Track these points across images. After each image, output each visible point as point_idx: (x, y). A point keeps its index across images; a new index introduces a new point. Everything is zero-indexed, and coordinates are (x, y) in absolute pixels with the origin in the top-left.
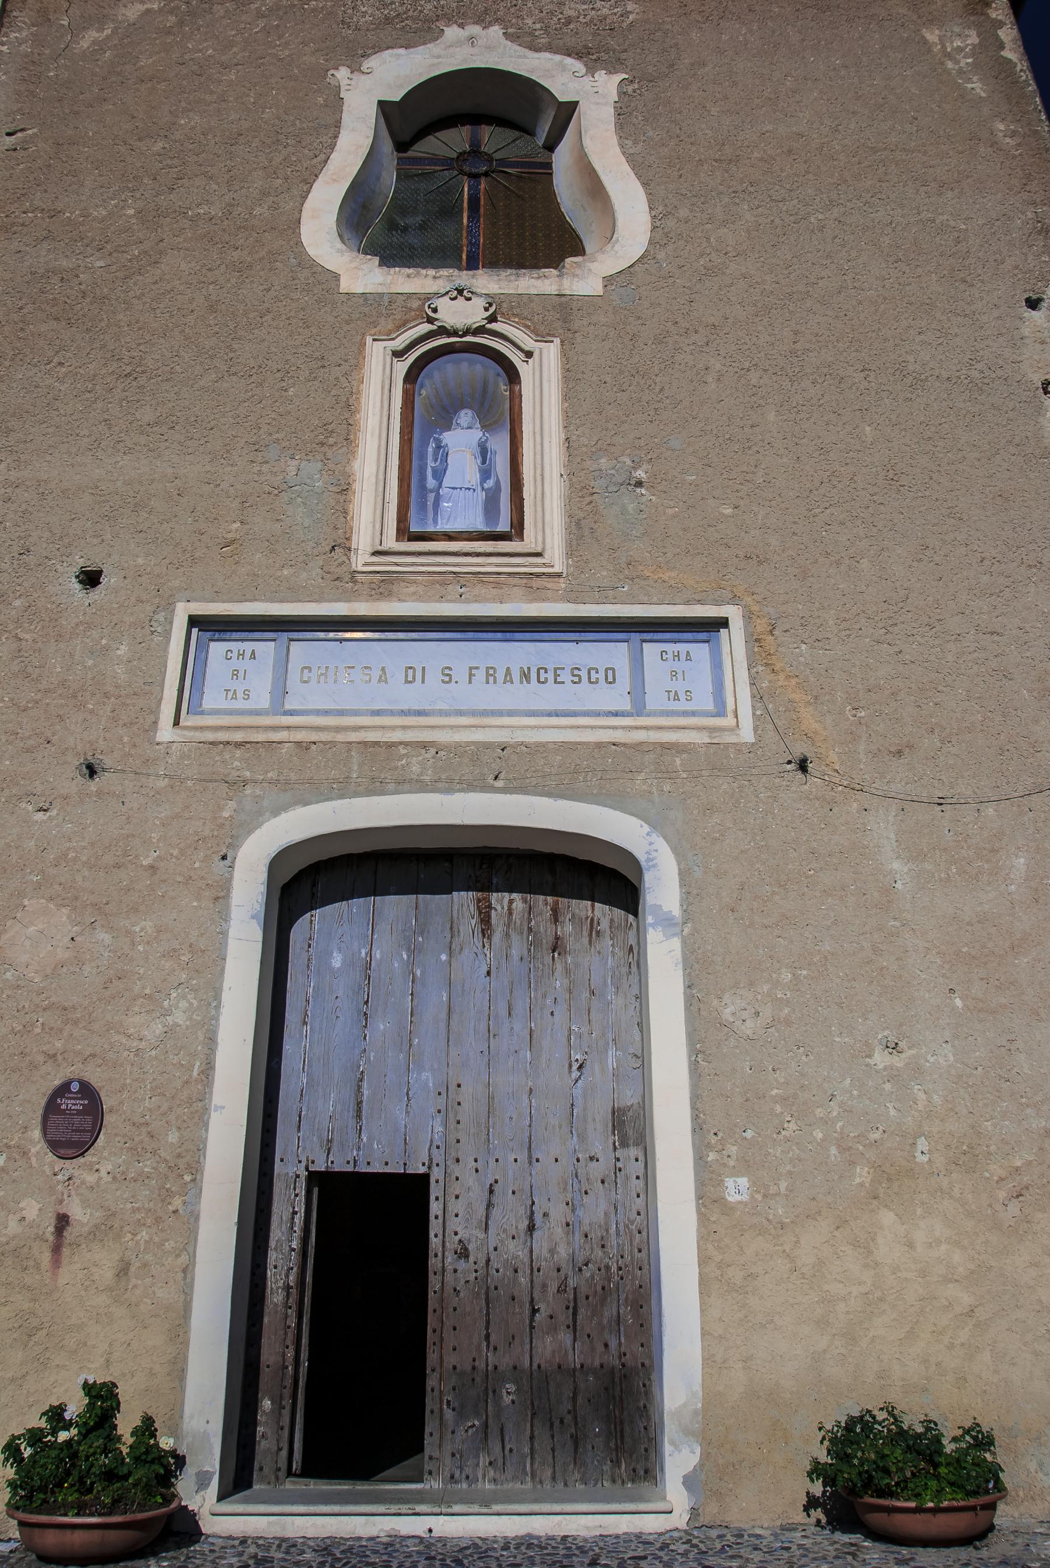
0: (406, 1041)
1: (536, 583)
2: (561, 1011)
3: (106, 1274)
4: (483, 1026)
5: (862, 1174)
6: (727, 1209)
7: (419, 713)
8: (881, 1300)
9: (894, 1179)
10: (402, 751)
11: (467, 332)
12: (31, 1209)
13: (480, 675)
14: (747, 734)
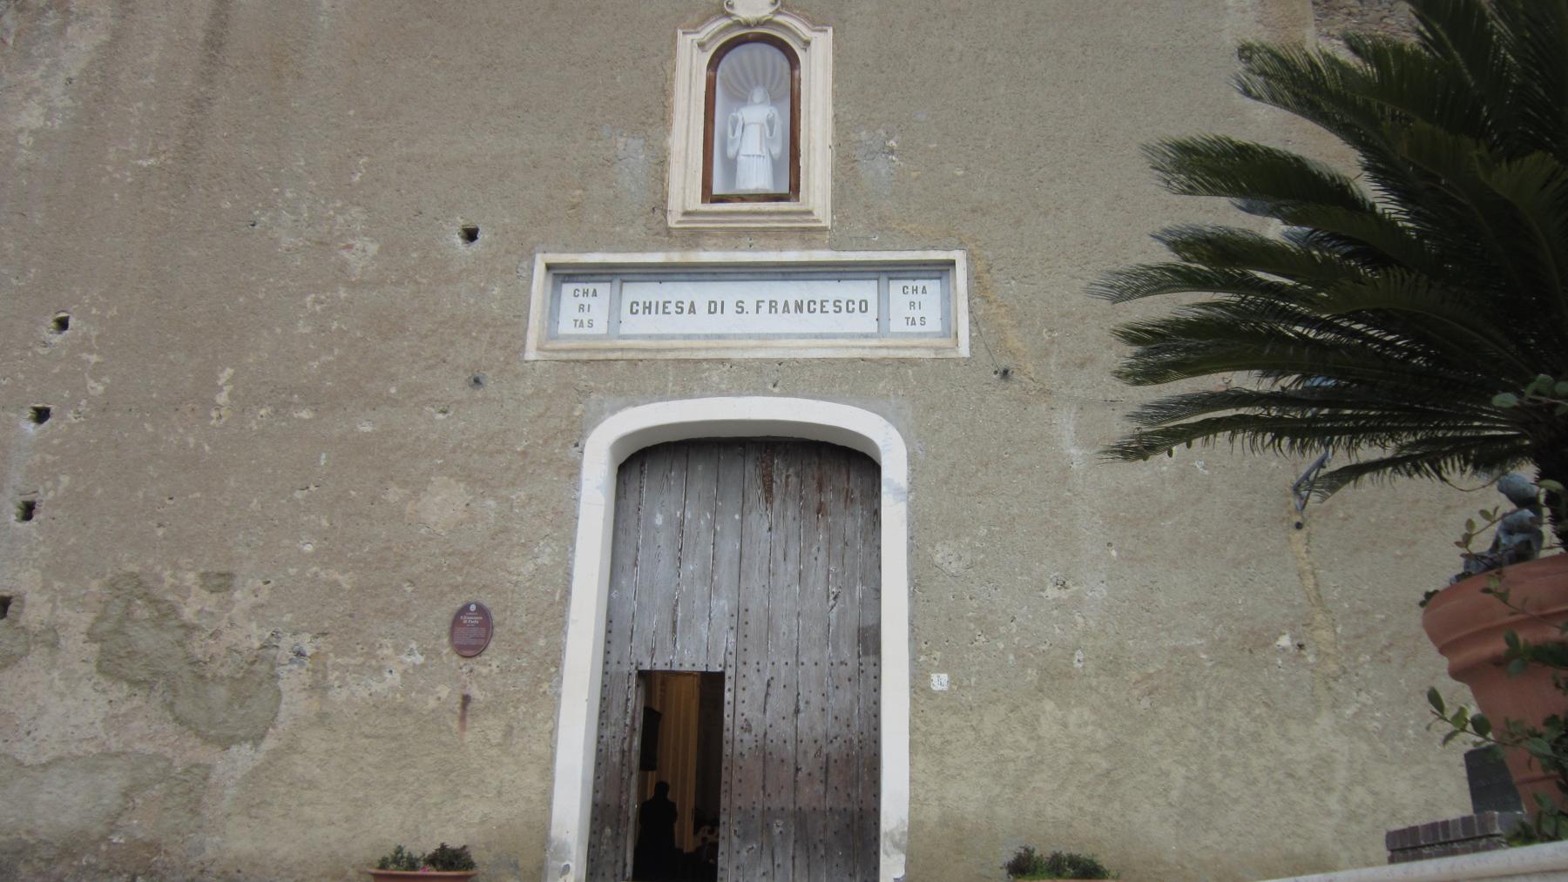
0: (709, 577)
1: (807, 236)
2: (822, 556)
3: (496, 736)
4: (765, 567)
5: (1032, 674)
6: (932, 695)
7: (720, 337)
8: (1041, 762)
9: (1056, 679)
10: (705, 366)
11: (759, 24)
12: (444, 691)
13: (765, 307)
14: (964, 351)
